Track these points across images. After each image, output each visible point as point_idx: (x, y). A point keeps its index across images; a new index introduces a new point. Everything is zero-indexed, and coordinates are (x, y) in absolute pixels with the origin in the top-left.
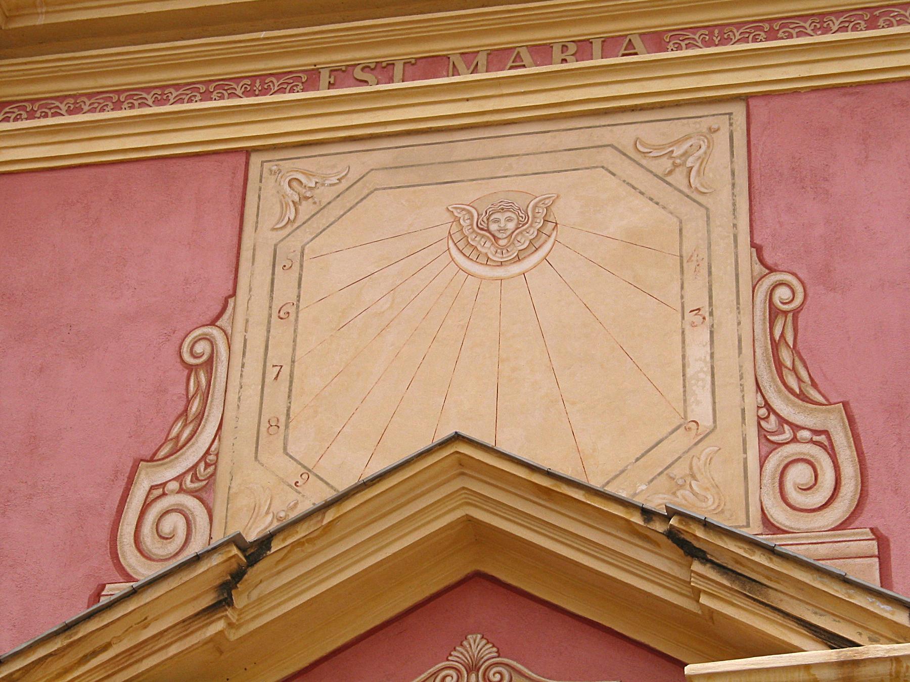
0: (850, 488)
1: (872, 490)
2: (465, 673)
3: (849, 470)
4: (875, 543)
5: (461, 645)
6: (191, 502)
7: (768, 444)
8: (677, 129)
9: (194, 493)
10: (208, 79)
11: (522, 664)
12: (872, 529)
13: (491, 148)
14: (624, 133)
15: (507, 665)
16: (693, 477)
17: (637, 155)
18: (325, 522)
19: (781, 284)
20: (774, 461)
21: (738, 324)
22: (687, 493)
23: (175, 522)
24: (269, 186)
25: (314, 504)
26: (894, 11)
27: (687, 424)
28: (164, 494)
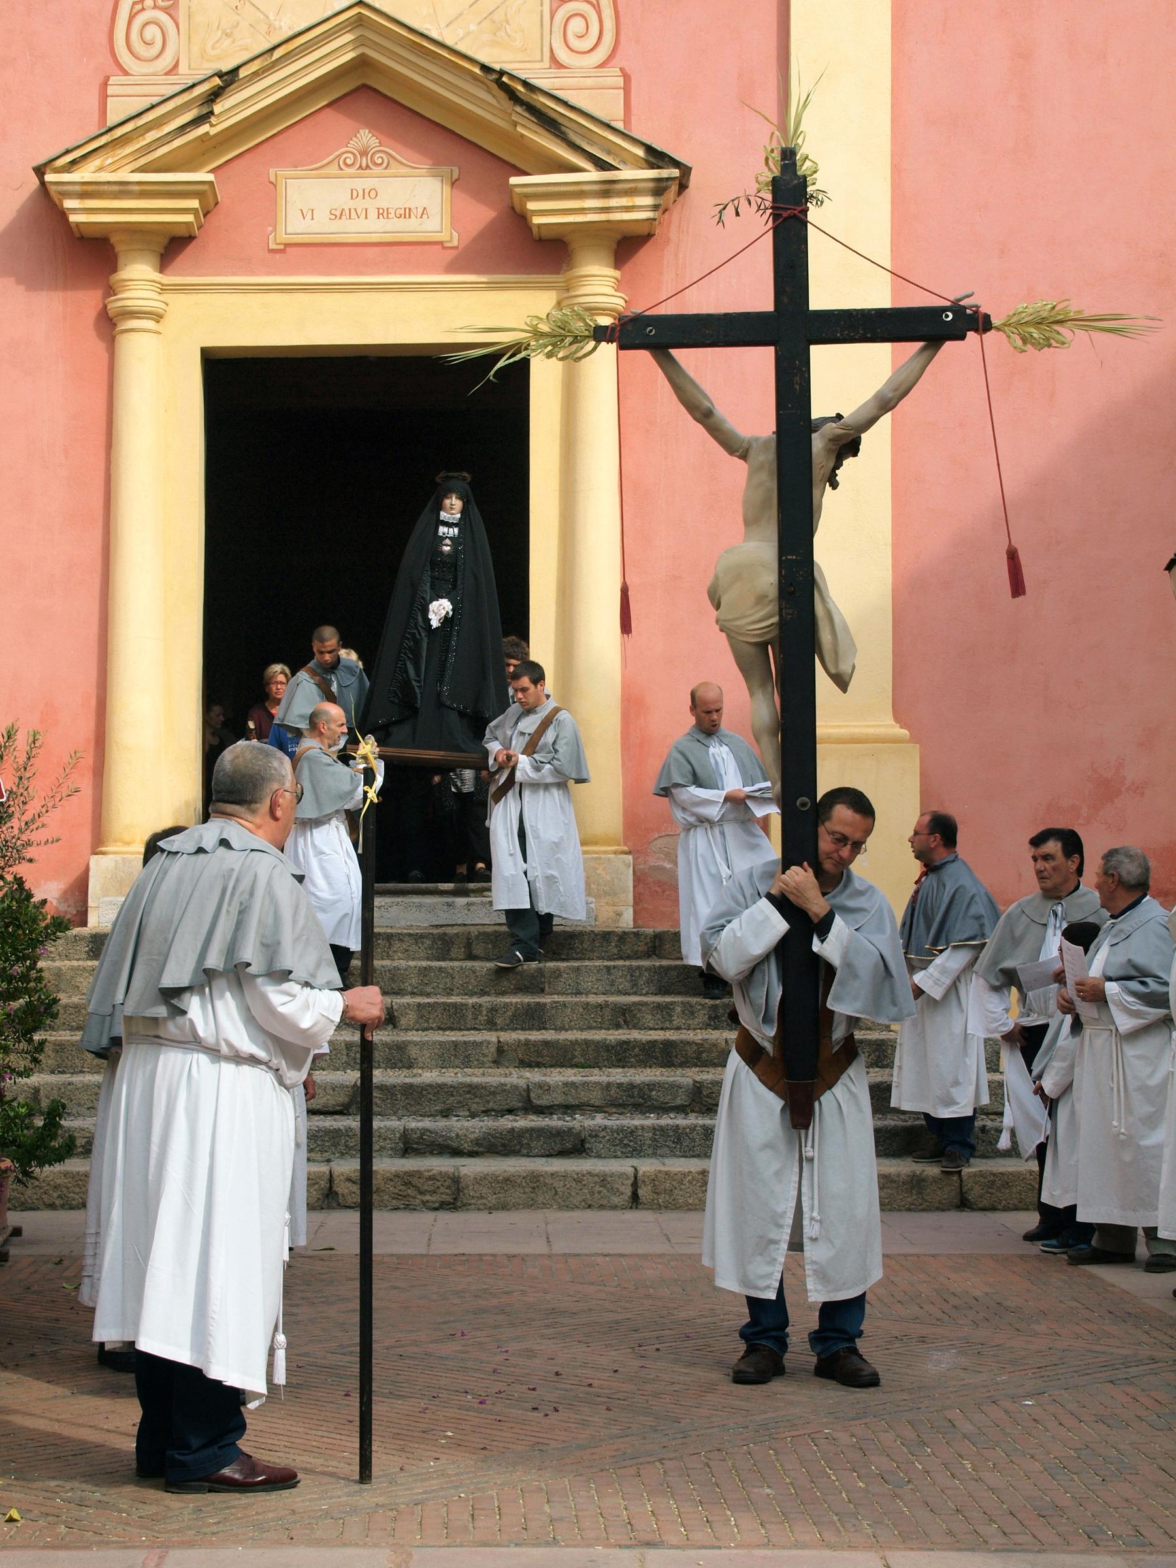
0: (609, 38)
1: (623, 38)
3: (609, 24)
4: (622, 79)
6: (163, 17)
9: (165, 10)
12: (622, 70)
16: (507, 22)
18: (274, 58)
22: (503, 34)
23: (152, 32)
28: (143, 9)
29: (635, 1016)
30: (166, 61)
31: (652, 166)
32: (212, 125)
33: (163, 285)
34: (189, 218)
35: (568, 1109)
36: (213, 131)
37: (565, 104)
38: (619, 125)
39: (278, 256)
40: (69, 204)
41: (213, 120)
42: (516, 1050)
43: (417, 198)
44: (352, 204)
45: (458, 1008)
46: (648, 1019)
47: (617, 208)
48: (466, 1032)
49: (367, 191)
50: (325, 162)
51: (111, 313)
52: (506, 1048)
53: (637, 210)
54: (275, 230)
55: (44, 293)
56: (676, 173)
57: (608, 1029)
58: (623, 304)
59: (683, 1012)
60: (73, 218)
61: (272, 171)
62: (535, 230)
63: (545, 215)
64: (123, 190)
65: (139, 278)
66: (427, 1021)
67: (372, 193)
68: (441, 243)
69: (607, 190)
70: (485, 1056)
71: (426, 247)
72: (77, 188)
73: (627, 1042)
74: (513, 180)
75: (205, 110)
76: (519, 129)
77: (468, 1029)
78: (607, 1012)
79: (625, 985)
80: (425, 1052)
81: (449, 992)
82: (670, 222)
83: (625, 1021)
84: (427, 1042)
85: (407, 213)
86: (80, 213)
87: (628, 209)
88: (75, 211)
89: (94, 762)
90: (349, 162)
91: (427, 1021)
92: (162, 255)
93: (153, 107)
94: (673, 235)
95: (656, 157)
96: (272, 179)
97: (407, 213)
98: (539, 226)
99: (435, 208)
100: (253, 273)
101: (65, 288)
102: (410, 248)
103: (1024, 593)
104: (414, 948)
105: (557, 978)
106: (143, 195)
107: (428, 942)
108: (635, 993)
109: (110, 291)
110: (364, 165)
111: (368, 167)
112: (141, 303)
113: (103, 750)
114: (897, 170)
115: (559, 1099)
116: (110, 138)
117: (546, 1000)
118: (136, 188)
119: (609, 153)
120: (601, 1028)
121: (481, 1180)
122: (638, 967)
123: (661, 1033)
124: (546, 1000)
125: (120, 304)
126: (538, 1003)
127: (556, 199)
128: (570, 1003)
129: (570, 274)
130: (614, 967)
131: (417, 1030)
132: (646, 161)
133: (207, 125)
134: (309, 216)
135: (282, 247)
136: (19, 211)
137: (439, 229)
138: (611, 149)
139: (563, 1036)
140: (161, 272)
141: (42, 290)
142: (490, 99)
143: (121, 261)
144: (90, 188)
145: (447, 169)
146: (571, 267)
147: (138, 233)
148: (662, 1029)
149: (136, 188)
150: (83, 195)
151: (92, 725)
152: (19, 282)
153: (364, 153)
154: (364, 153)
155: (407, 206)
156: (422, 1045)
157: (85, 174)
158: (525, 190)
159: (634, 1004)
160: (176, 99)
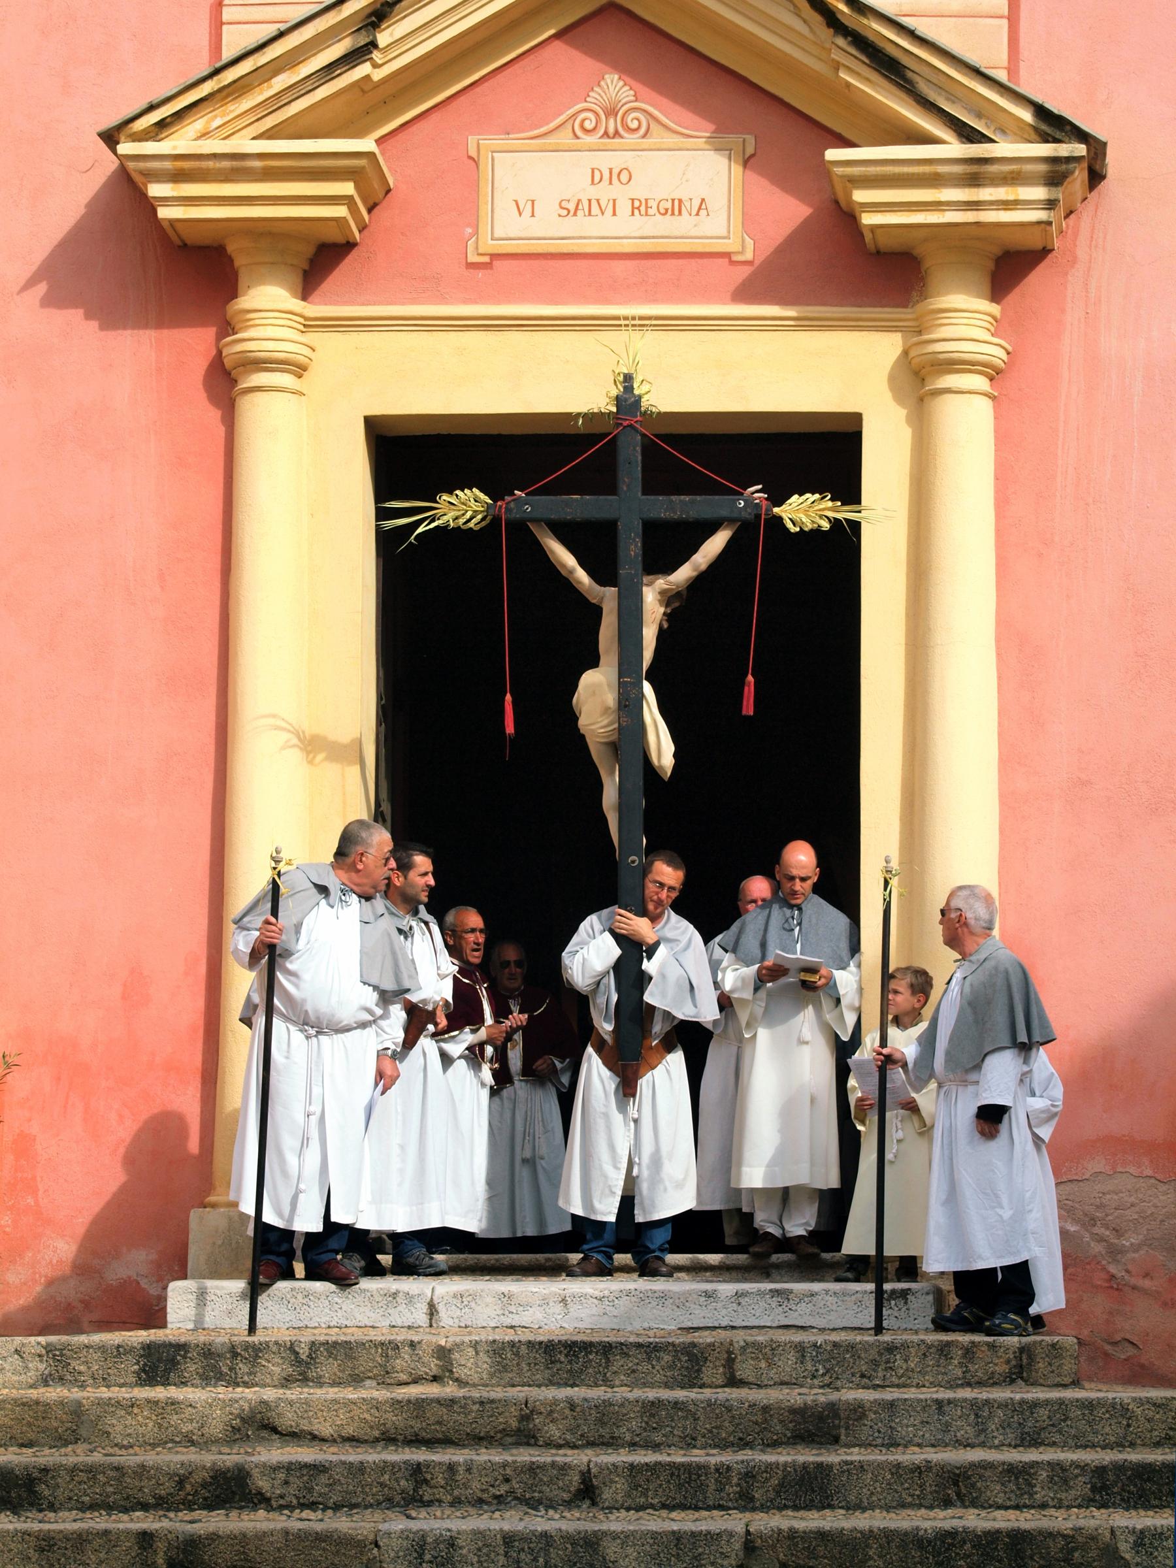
2: (603, 117)
5: (599, 85)
10: (927, 169)
11: (660, 111)
15: (645, 111)
19: (583, 121)
29: (973, 1485)
31: (1046, 139)
32: (376, 66)
33: (306, 319)
34: (341, 211)
36: (378, 75)
37: (911, 34)
38: (1002, 76)
39: (480, 274)
40: (155, 190)
41: (376, 56)
42: (773, 1547)
43: (689, 184)
44: (593, 192)
45: (693, 1472)
46: (996, 1491)
47: (992, 203)
48: (705, 1513)
49: (615, 173)
50: (552, 125)
51: (228, 363)
52: (758, 1542)
53: (1020, 207)
54: (476, 232)
55: (128, 332)
56: (1080, 149)
57: (931, 1508)
58: (1004, 356)
59: (1051, 1479)
60: (164, 213)
61: (472, 140)
62: (868, 237)
63: (883, 211)
64: (236, 167)
65: (270, 308)
66: (644, 1494)
67: (622, 176)
68: (727, 255)
69: (976, 173)
70: (725, 1556)
71: (705, 261)
72: (168, 165)
73: (952, 1534)
74: (832, 154)
75: (362, 40)
76: (843, 75)
77: (709, 1508)
78: (930, 1480)
79: (967, 1431)
80: (630, 1550)
81: (689, 1442)
82: (1076, 234)
83: (958, 1494)
84: (633, 1533)
85: (676, 208)
86: (175, 203)
87: (1007, 205)
88: (165, 201)
89: (204, 1062)
90: (588, 125)
91: (644, 1494)
92: (305, 272)
93: (281, 35)
94: (1082, 253)
95: (1052, 124)
96: (473, 152)
97: (676, 208)
98: (873, 228)
99: (718, 202)
100: (443, 300)
101: (159, 325)
102: (681, 262)
103: (857, 418)
104: (645, 1367)
105: (860, 1418)
106: (268, 175)
107: (667, 1358)
108: (983, 1445)
109: (227, 327)
110: (611, 131)
111: (617, 133)
112: (270, 345)
113: (217, 1042)
116: (220, 82)
117: (833, 1457)
118: (257, 164)
119: (979, 116)
120: (920, 1506)
122: (987, 1402)
123: (1012, 1514)
124: (833, 1457)
125: (239, 348)
126: (820, 1465)
127: (900, 187)
128: (870, 1463)
129: (921, 307)
130: (949, 1402)
131: (628, 1509)
132: (1036, 129)
133: (368, 64)
134: (527, 212)
135: (486, 259)
136: (88, 206)
137: (725, 234)
138: (983, 109)
139: (863, 1521)
140: (305, 297)
141: (125, 328)
142: (804, 30)
143: (243, 280)
144: (186, 165)
145: (735, 139)
146: (924, 295)
147: (269, 236)
148: (1017, 1507)
149: (257, 164)
150: (178, 177)
151: (201, 1003)
152: (88, 316)
153: (611, 112)
154: (611, 112)
155: (677, 196)
156: (625, 1538)
157: (180, 141)
158: (849, 170)
159: (973, 1465)
160: (317, 21)
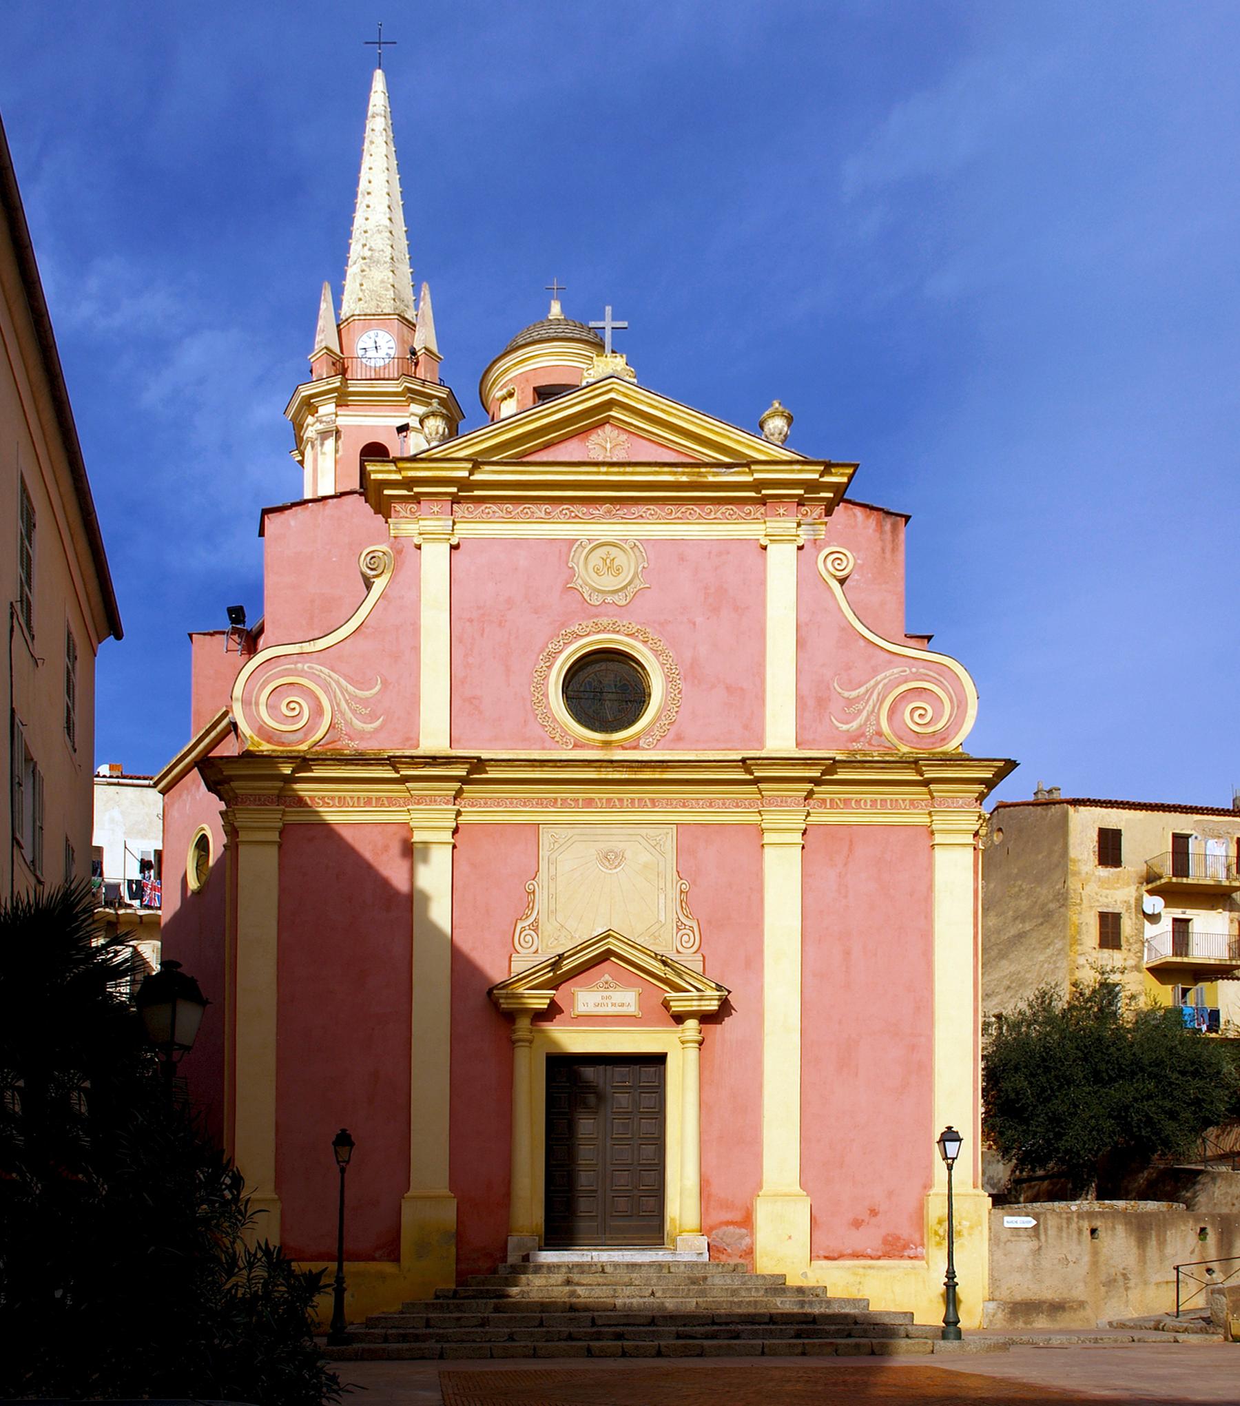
7: (679, 929)
8: (660, 831)
13: (607, 831)
14: (644, 831)
17: (646, 838)
20: (680, 933)
21: (673, 893)
23: (529, 938)
24: (545, 837)
25: (1142, 1229)
26: (877, 684)
27: (658, 921)
30: (534, 948)
35: (727, 1324)
85: (622, 1005)
97: (622, 1005)
109: (514, 1031)
114: (279, 907)
115: (724, 1320)
121: (710, 1347)
150: (506, 998)
